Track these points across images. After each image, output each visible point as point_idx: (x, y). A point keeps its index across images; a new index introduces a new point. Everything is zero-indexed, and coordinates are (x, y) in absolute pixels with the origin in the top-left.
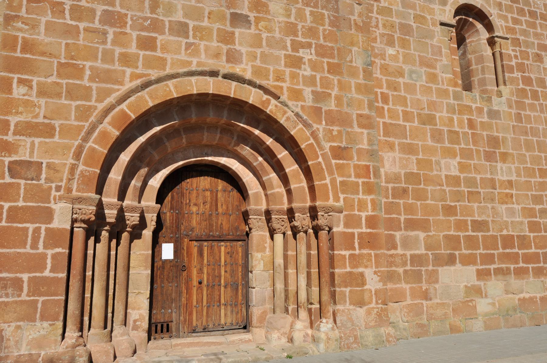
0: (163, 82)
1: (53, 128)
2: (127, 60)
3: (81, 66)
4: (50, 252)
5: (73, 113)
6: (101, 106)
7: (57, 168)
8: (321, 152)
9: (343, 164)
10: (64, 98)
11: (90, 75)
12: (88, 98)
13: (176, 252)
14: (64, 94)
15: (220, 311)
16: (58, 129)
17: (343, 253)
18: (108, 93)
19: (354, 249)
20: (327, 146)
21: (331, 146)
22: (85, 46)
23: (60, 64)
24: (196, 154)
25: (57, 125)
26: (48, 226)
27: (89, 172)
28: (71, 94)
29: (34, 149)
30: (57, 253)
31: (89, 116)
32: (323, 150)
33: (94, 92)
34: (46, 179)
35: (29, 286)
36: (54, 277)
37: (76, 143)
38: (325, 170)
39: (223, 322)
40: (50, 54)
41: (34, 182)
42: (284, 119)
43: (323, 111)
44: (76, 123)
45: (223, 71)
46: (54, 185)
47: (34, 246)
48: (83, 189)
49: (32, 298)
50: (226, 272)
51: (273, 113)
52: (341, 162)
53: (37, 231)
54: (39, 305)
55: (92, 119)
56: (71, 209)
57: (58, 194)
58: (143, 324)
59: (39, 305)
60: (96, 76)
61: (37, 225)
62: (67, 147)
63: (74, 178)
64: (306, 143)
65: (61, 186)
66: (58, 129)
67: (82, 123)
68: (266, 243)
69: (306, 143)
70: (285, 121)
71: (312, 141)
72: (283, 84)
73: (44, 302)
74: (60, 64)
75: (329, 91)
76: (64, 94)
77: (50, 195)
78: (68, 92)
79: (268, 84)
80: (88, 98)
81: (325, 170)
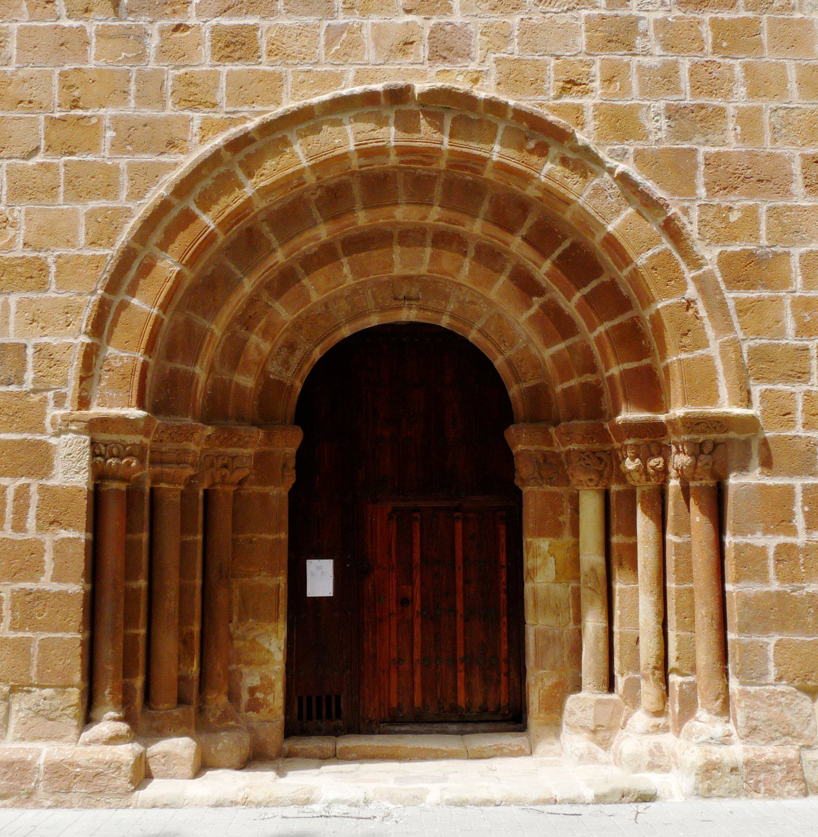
0: (274, 132)
1: (43, 269)
2: (193, 94)
3: (94, 121)
4: (48, 540)
5: (82, 230)
6: (141, 209)
7: (57, 356)
8: (694, 273)
9: (760, 300)
10: (61, 197)
11: (113, 138)
12: (109, 189)
13: (297, 579)
14: (61, 189)
15: (455, 676)
16: (53, 269)
17: (758, 540)
18: (151, 174)
19: (793, 532)
20: (710, 254)
21: (721, 253)
22: (100, 72)
23: (52, 122)
24: (380, 300)
25: (50, 260)
26: (44, 482)
27: (121, 359)
28: (80, 185)
29: (7, 317)
30: (63, 540)
31: (117, 230)
32: (700, 267)
33: (124, 179)
34: (35, 381)
35: (13, 609)
36: (60, 593)
37: (94, 298)
38: (706, 321)
39: (462, 700)
40: (30, 102)
41: (12, 388)
42: (588, 191)
43: (700, 158)
44: (88, 253)
45: (420, 87)
46: (50, 395)
47: (19, 527)
48: (111, 398)
49: (20, 634)
50: (466, 582)
51: (554, 181)
52: (754, 294)
53: (22, 494)
54: (35, 650)
55: (123, 237)
56: (87, 443)
57: (62, 412)
58: (270, 698)
59: (35, 650)
60: (130, 136)
61: (24, 480)
62: (69, 310)
63: (92, 375)
64: (650, 252)
65: (64, 396)
66: (53, 269)
67: (101, 252)
68: (562, 513)
69: (650, 252)
70: (591, 197)
71: (666, 244)
72: (588, 102)
73: (44, 646)
74: (52, 122)
75: (717, 102)
76: (61, 189)
77: (43, 415)
78: (69, 182)
79: (541, 105)
80: (109, 189)
81: (706, 321)
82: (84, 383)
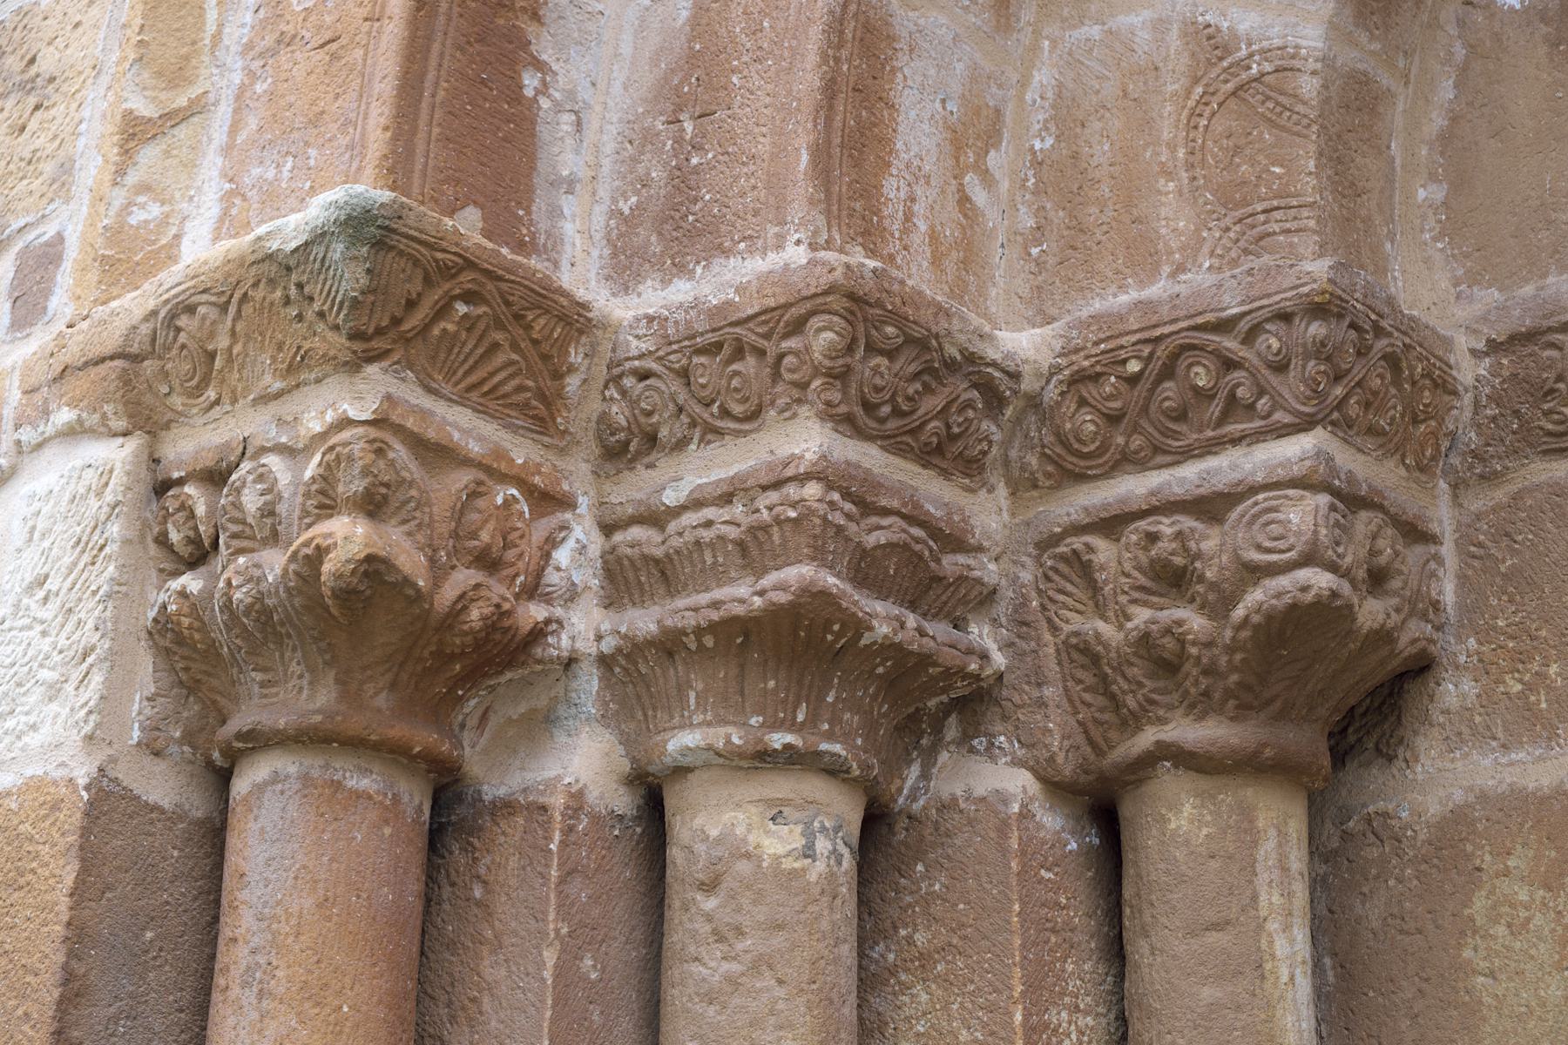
63: (197, 108)
82: (149, 155)
